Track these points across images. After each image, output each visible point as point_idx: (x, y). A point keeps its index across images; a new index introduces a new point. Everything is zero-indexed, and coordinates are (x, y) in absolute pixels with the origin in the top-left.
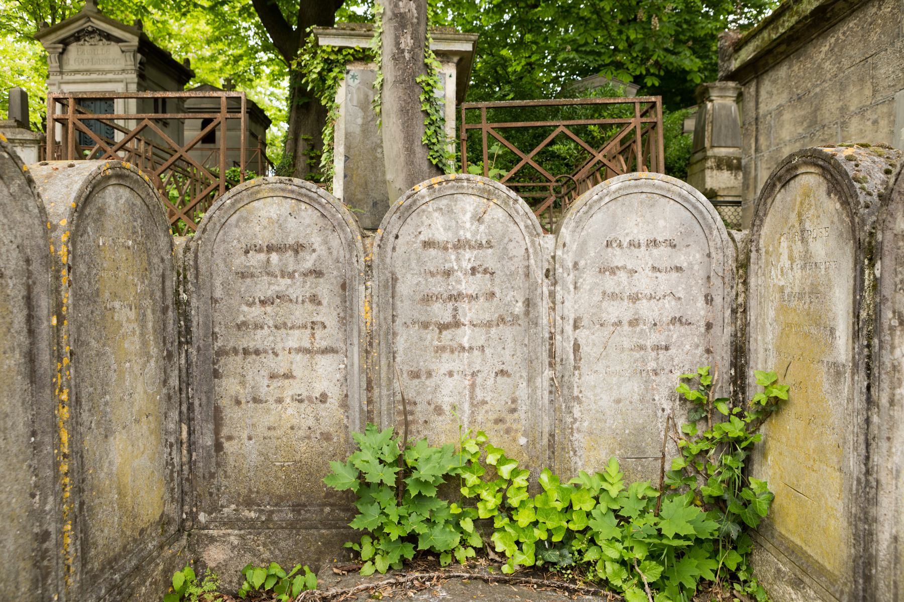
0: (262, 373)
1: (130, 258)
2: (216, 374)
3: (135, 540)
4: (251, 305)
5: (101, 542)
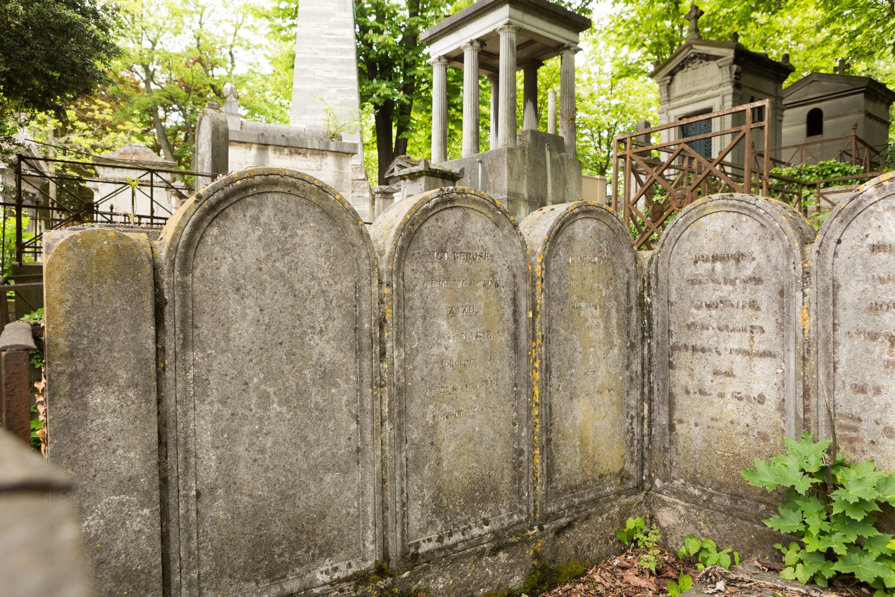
0: (707, 368)
1: (596, 271)
2: (671, 366)
3: (594, 480)
4: (699, 308)
5: (564, 471)
